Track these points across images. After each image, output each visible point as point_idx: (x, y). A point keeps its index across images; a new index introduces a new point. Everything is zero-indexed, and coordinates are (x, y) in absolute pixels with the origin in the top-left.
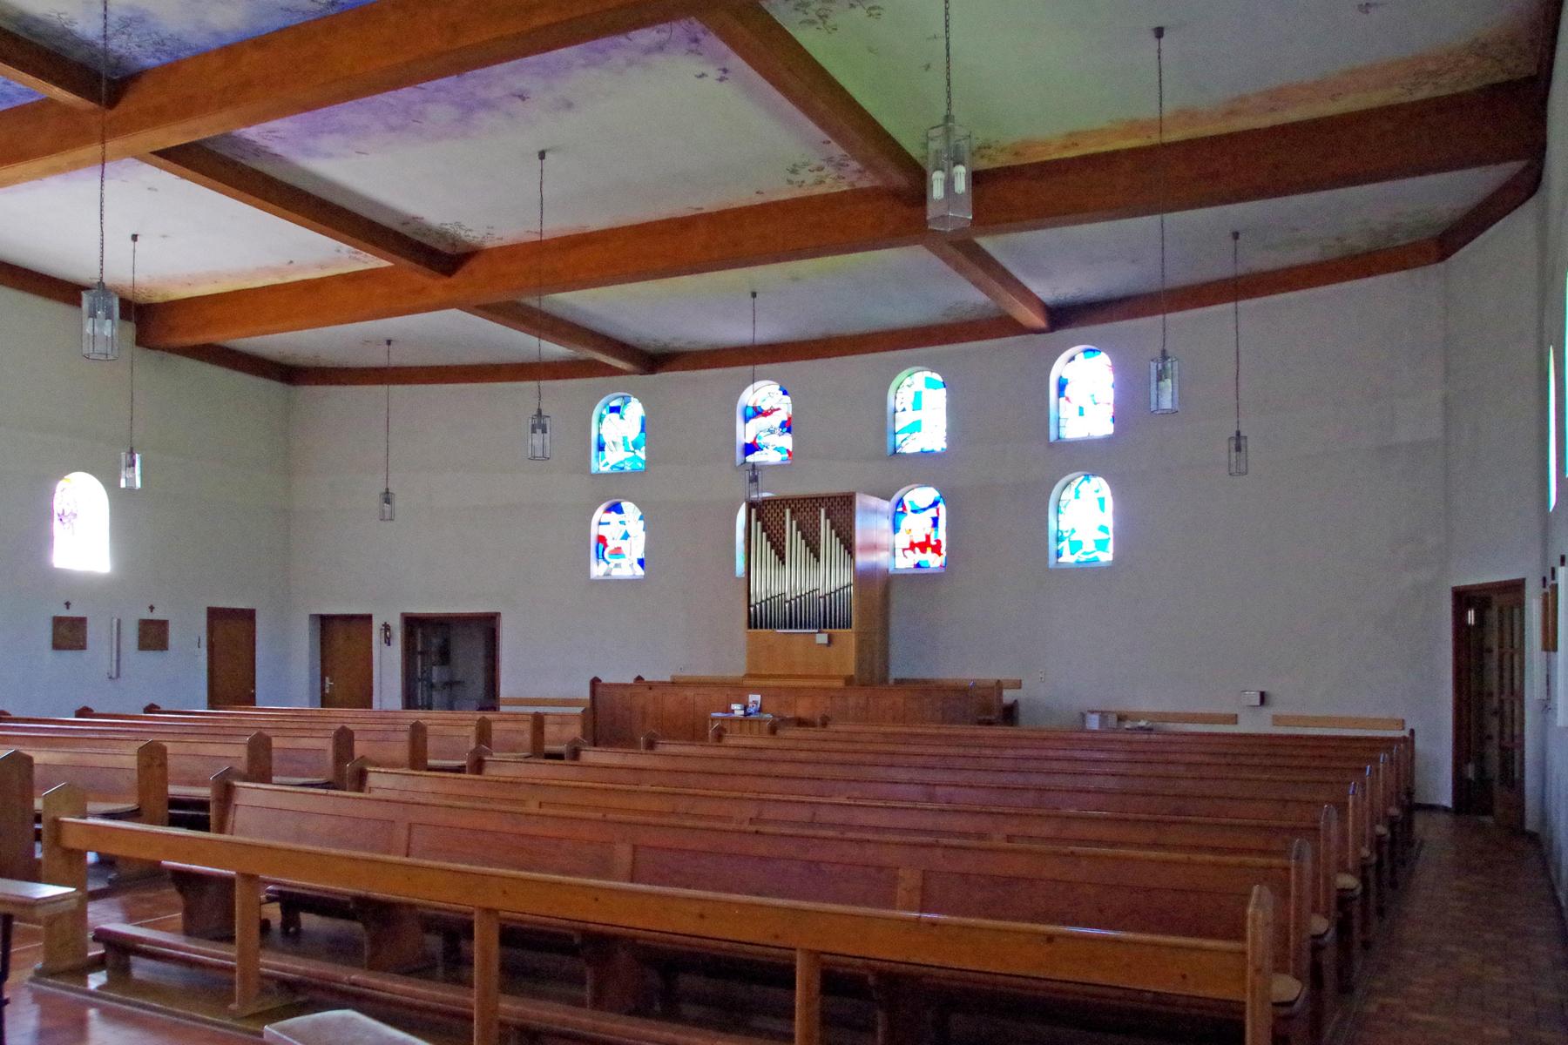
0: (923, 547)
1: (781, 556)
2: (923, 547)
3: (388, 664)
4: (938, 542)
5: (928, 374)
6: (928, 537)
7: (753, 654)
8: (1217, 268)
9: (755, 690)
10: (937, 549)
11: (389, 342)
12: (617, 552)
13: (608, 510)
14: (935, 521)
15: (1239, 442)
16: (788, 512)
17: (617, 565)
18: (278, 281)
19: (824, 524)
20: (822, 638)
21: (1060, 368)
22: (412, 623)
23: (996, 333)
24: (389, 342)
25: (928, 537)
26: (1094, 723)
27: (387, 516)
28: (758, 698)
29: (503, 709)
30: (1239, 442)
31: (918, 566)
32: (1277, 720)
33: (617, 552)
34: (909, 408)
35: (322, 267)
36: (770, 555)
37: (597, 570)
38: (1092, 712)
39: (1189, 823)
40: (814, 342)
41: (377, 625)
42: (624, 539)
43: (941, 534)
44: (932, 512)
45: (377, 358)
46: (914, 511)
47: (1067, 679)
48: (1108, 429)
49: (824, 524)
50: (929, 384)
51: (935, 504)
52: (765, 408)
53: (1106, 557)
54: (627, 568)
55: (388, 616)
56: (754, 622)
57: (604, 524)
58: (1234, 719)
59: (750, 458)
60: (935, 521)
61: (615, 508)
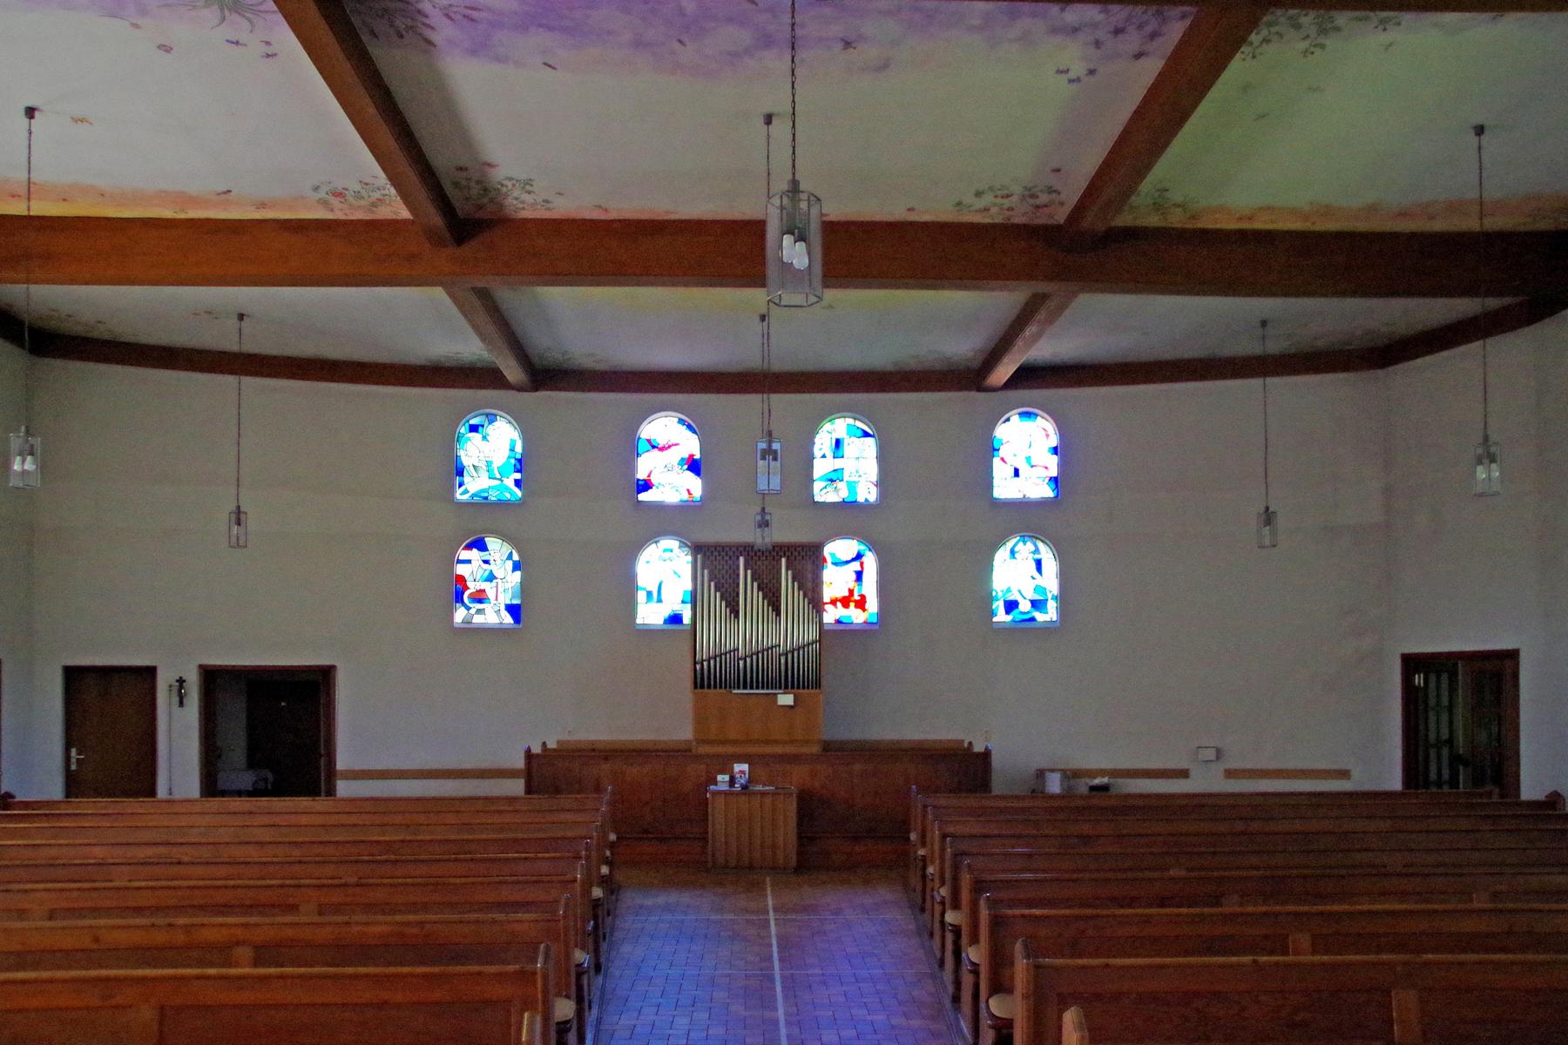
0: (845, 602)
1: (774, 604)
2: (845, 602)
3: (179, 735)
4: (863, 597)
5: (851, 421)
6: (851, 592)
7: (700, 720)
8: (1246, 346)
9: (741, 759)
10: (861, 604)
11: (241, 317)
12: (480, 597)
13: (469, 547)
14: (859, 575)
15: (1268, 517)
16: (742, 559)
17: (479, 611)
18: (167, 213)
19: (785, 576)
20: (786, 699)
21: (1002, 431)
22: (212, 677)
23: (757, 391)
24: (241, 317)
25: (851, 592)
26: (1054, 785)
27: (1267, 542)
28: (745, 767)
29: (344, 788)
30: (1268, 517)
31: (838, 622)
32: (1230, 774)
33: (480, 597)
34: (829, 454)
35: (262, 205)
36: (720, 606)
37: (1050, 614)
38: (1053, 771)
39: (505, 882)
40: (730, 374)
41: (164, 681)
42: (494, 577)
43: (870, 588)
44: (856, 566)
45: (223, 338)
46: (835, 564)
47: (1033, 738)
48: (1047, 492)
49: (785, 576)
50: (851, 431)
51: (859, 556)
52: (662, 442)
53: (639, 621)
54: (493, 615)
55: (177, 668)
56: (701, 682)
57: (470, 566)
58: (1184, 774)
59: (643, 497)
60: (859, 575)
61: (480, 545)
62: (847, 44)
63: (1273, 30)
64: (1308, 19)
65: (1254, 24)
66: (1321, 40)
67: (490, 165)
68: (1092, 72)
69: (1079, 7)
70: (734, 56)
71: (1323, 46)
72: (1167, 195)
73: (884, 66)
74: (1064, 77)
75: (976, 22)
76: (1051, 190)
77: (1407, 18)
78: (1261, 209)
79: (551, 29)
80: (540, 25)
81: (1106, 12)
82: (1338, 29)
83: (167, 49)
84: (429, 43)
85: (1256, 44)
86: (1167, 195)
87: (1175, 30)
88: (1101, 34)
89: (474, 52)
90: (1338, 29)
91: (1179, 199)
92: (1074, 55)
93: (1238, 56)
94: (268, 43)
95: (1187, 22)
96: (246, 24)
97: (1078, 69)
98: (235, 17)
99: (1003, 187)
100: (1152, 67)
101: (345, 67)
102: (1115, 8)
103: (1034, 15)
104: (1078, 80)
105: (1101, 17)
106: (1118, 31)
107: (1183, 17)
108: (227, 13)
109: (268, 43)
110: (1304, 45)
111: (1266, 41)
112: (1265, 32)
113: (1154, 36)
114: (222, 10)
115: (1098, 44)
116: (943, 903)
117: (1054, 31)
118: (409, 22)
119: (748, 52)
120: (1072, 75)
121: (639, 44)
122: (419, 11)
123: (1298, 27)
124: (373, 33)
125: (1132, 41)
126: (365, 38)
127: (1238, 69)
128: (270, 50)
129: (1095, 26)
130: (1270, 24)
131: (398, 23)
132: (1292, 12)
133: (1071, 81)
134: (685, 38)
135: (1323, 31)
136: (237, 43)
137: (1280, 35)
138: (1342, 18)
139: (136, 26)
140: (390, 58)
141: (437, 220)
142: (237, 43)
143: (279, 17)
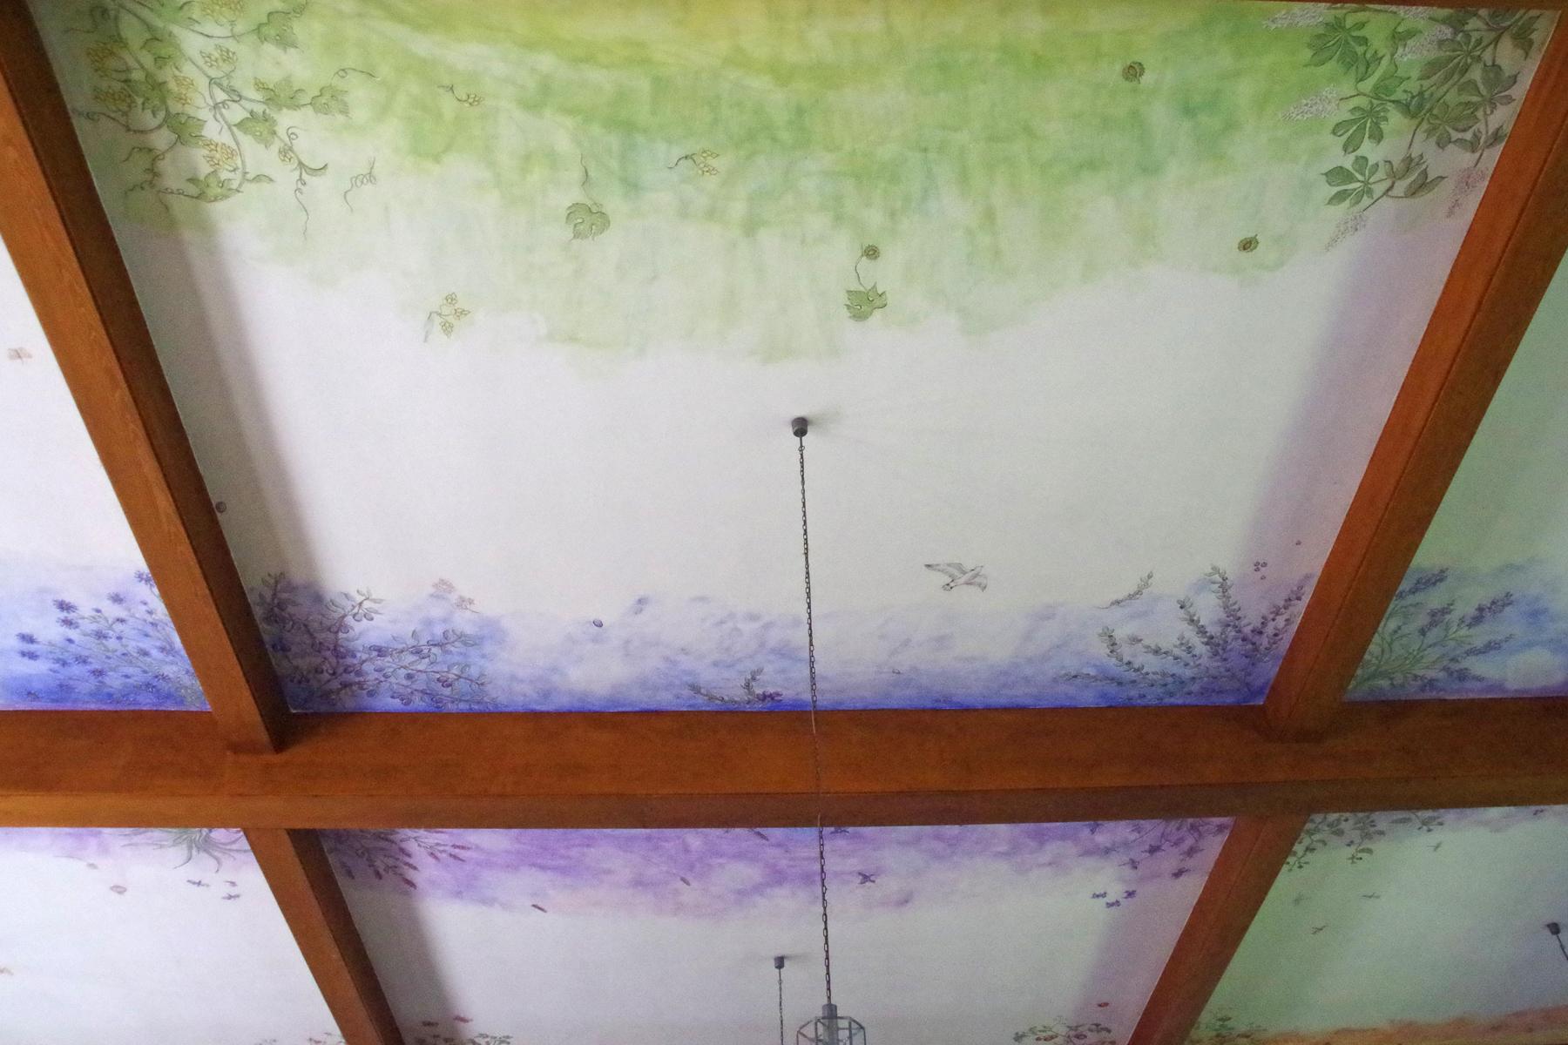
62: (866, 878)
63: (1317, 837)
64: (1349, 822)
65: (1293, 838)
66: (1367, 844)
67: (464, 1020)
68: (1130, 894)
69: (1110, 825)
70: (744, 894)
71: (1369, 851)
72: (1229, 1024)
73: (905, 901)
74: (1103, 901)
75: (1004, 848)
76: (1098, 1027)
77: (1450, 816)
78: (1337, 1032)
79: (543, 868)
80: (534, 865)
81: (1138, 829)
82: (1382, 833)
83: (119, 890)
84: (411, 884)
85: (1300, 853)
86: (1229, 1024)
87: (1213, 846)
88: (1135, 854)
89: (458, 894)
90: (1382, 833)
91: (1243, 1029)
92: (1109, 878)
93: (1285, 868)
94: (233, 884)
95: (1225, 837)
96: (213, 863)
97: (1116, 891)
98: (203, 855)
99: (1045, 1028)
100: (1192, 888)
101: (326, 939)
102: (1146, 824)
103: (1063, 838)
104: (1117, 903)
105: (1134, 836)
106: (1153, 850)
107: (1221, 828)
108: (194, 852)
109: (233, 884)
110: (1352, 850)
111: (1309, 849)
112: (1306, 841)
113: (1191, 852)
114: (190, 848)
115: (1134, 865)
116: (792, 859)
117: (1088, 853)
118: (391, 862)
119: (758, 889)
120: (1111, 898)
121: (639, 883)
122: (402, 850)
123: (1340, 833)
124: (350, 874)
125: (1169, 860)
126: (341, 880)
127: (1286, 882)
128: (233, 891)
129: (1126, 844)
130: (1310, 833)
131: (378, 863)
132: (1333, 817)
133: (1109, 905)
134: (689, 878)
135: (1367, 836)
136: (199, 883)
137: (1325, 843)
138: (1382, 820)
139: (92, 866)
140: (362, 900)
141: (245, 707)
142: (199, 883)
143: (251, 858)
